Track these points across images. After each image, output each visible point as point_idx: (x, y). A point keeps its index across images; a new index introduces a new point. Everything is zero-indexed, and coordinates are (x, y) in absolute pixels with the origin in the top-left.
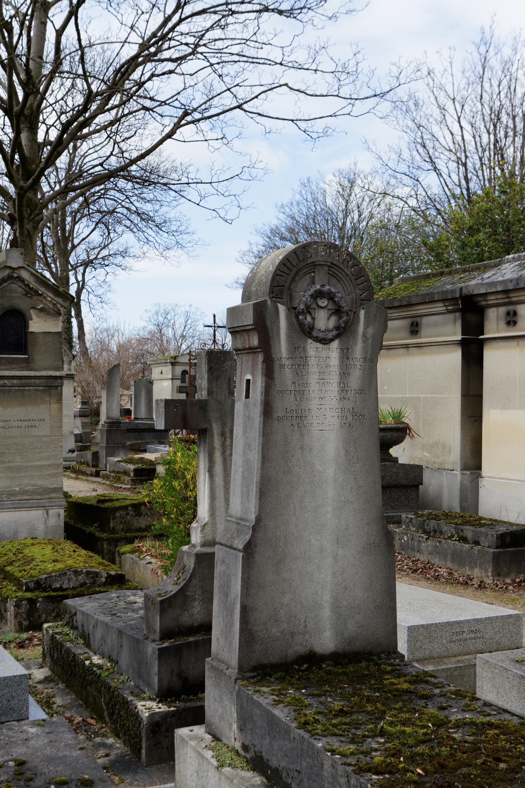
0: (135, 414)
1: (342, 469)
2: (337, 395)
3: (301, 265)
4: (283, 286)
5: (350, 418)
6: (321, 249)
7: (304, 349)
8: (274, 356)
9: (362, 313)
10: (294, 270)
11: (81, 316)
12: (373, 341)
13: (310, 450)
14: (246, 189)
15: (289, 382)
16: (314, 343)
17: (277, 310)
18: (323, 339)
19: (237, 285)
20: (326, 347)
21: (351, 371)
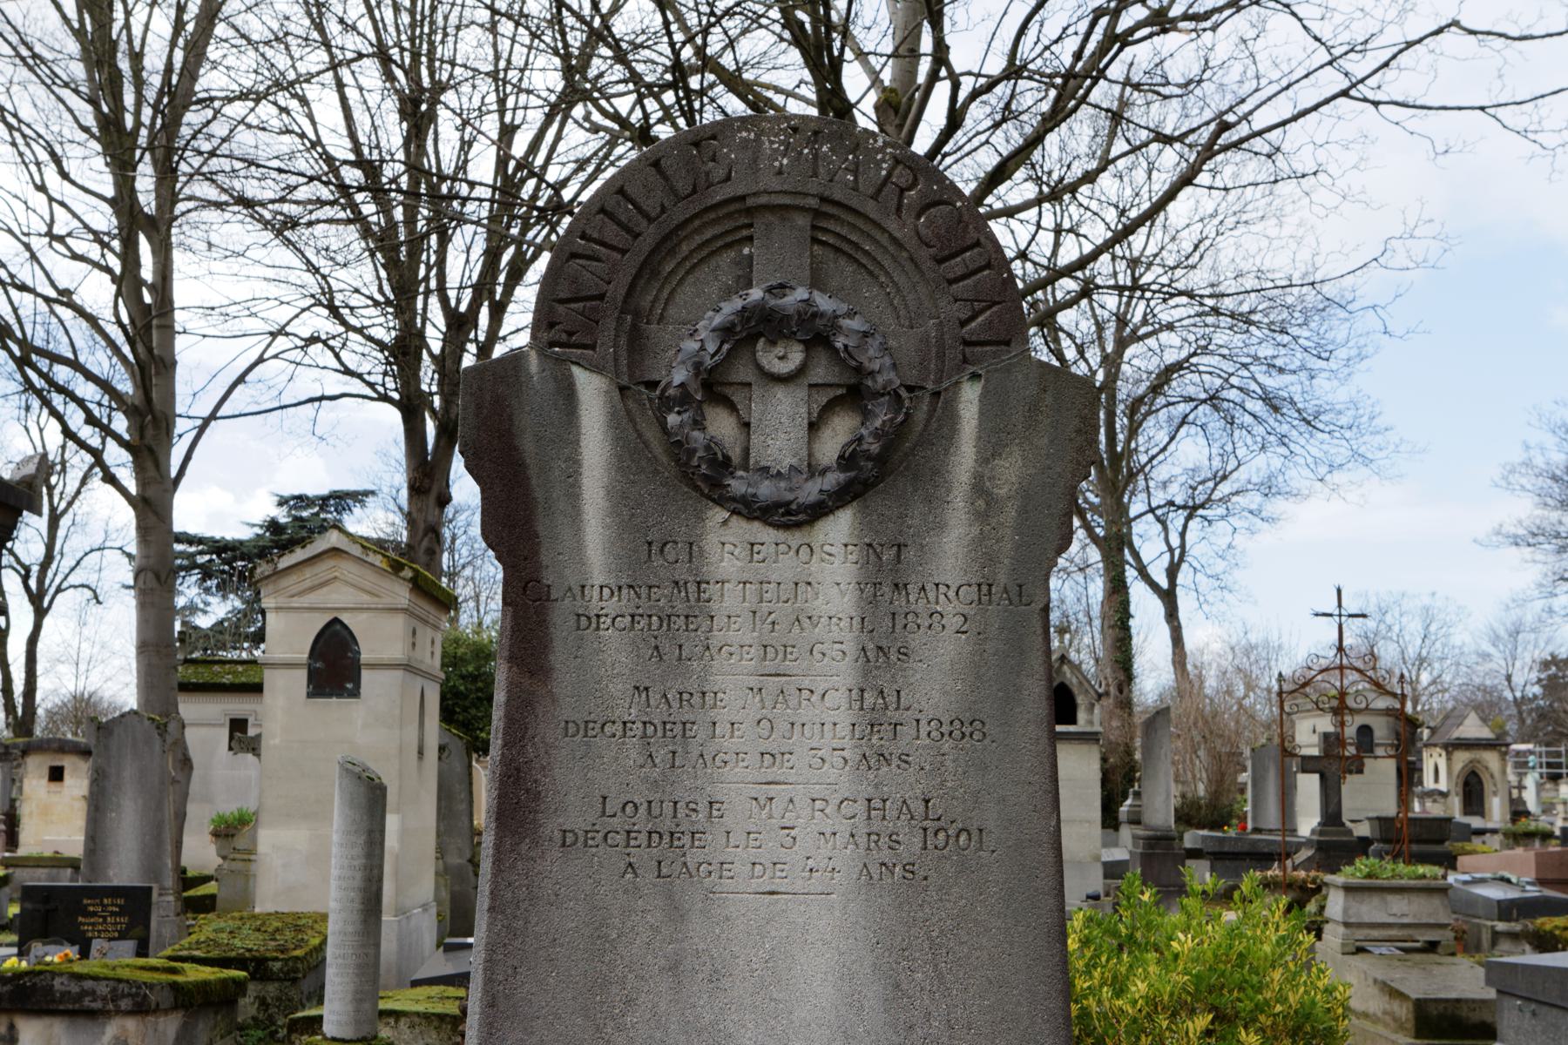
0: (1254, 819)
2: (847, 743)
3: (679, 214)
4: (601, 297)
5: (911, 844)
7: (693, 549)
8: (549, 578)
9: (970, 398)
10: (650, 235)
12: (1023, 511)
13: (715, 977)
14: (1401, 291)
16: (736, 522)
17: (568, 393)
18: (778, 505)
19: (1500, 538)
20: (795, 538)
21: (916, 640)
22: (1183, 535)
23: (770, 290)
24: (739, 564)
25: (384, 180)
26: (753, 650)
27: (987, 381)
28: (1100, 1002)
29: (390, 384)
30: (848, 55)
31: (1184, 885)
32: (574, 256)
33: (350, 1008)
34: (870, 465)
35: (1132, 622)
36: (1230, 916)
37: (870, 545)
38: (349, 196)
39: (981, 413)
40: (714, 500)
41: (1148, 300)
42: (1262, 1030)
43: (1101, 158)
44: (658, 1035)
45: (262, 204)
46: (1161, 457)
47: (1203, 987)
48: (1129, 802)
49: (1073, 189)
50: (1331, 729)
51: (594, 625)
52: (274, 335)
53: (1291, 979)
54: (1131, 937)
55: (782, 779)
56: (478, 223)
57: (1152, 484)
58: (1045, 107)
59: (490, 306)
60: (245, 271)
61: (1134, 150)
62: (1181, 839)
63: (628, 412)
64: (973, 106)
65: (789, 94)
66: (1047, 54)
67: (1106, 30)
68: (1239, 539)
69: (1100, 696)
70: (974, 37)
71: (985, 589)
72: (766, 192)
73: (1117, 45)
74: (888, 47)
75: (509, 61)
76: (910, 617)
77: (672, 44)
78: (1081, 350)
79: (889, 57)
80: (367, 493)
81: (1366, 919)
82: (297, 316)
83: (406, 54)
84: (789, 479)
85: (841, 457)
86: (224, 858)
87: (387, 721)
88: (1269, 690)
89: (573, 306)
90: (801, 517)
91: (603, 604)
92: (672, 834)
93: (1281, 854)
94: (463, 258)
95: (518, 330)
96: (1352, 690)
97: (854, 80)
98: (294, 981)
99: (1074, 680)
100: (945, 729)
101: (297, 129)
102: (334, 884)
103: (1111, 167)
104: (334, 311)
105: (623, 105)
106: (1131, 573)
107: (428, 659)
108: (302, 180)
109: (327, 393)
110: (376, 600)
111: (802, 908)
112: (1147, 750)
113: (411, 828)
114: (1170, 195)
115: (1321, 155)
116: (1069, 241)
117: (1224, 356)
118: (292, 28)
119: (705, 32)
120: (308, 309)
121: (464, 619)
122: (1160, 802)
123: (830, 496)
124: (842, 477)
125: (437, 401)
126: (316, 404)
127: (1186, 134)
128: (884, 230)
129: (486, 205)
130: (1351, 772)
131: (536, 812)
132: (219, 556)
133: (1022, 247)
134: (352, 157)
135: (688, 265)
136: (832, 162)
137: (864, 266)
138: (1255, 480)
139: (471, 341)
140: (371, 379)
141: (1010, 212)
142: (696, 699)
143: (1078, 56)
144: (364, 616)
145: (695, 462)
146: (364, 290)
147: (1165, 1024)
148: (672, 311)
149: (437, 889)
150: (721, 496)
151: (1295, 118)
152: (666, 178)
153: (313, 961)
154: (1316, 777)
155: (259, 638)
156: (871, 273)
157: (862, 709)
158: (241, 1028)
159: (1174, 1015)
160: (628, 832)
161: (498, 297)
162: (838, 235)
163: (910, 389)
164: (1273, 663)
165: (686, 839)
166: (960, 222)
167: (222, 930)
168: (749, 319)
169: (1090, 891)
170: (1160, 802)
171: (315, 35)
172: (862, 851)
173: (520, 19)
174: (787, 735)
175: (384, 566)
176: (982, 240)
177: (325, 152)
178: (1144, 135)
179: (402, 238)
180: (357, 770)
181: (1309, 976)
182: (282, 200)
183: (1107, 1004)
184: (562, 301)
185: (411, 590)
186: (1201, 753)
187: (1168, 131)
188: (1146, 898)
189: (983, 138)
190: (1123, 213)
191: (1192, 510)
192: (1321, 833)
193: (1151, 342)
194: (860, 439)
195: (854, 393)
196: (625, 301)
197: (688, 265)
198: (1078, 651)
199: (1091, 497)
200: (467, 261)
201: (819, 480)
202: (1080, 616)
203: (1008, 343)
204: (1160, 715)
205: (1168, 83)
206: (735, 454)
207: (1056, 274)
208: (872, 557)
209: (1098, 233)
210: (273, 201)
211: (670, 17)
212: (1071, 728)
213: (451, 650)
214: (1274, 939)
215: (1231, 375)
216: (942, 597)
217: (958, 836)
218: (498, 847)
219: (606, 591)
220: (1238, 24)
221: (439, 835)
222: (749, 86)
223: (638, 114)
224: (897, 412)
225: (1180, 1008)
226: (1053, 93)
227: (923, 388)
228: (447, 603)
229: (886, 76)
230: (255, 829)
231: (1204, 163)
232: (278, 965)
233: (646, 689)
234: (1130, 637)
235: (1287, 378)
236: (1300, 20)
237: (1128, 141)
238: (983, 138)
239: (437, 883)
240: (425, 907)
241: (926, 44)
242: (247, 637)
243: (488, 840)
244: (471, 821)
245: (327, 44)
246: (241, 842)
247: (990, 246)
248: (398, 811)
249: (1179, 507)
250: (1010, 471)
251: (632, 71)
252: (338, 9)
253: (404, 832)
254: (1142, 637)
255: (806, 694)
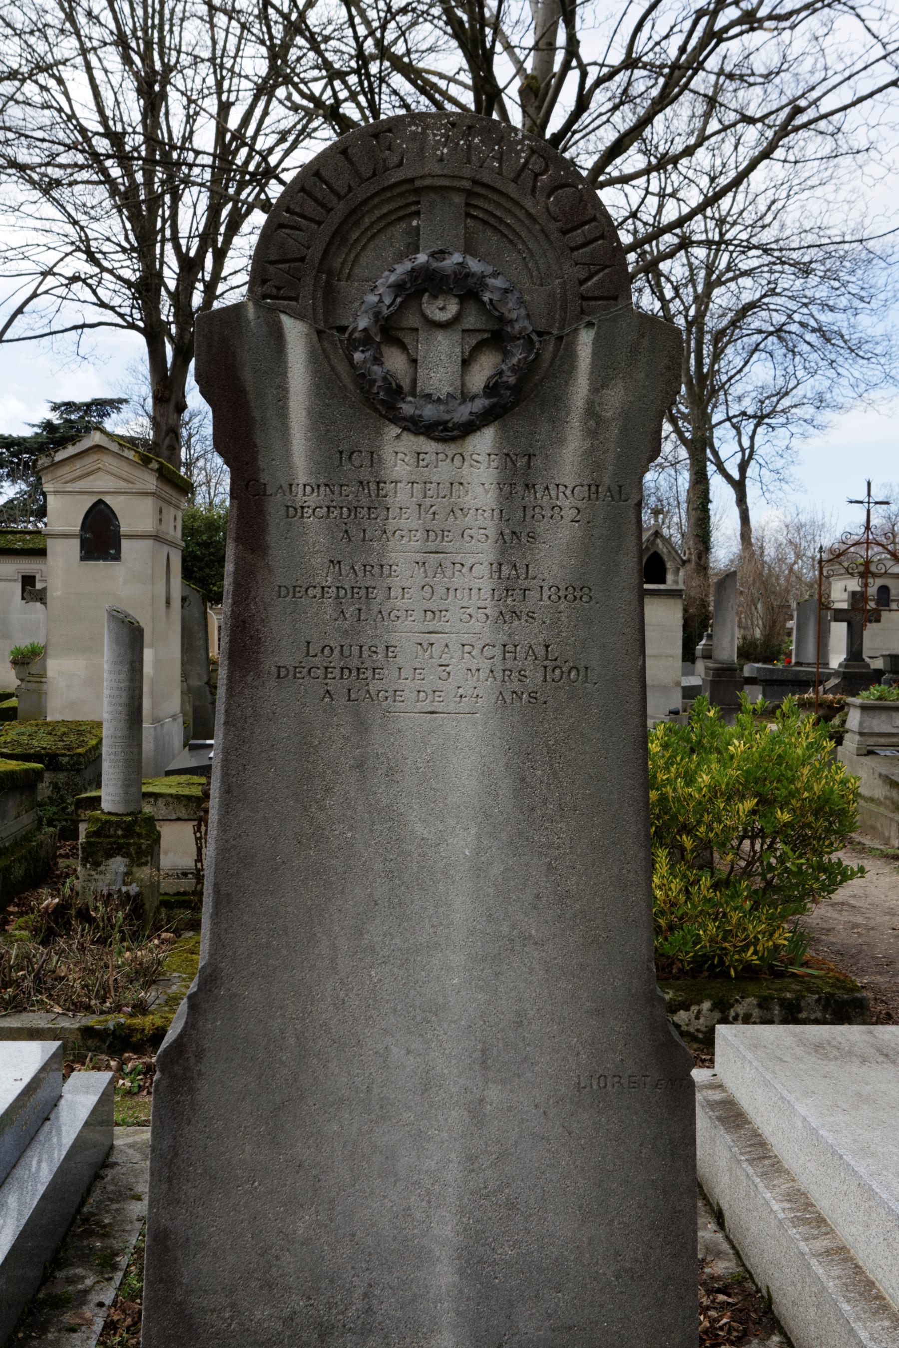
0: (797, 655)
1: (504, 836)
2: (489, 603)
3: (362, 193)
4: (302, 259)
5: (535, 677)
6: (435, 136)
7: (374, 458)
8: (265, 478)
9: (585, 341)
10: (340, 209)
11: (745, 503)
12: (624, 430)
13: (390, 772)
15: (318, 561)
16: (406, 436)
17: (278, 336)
20: (451, 449)
21: (541, 527)
22: (752, 438)
23: (432, 255)
24: (408, 468)
25: (128, 148)
26: (419, 534)
27: (599, 328)
28: (675, 790)
29: (137, 316)
30: (499, 47)
31: (741, 705)
32: (281, 226)
33: (121, 791)
34: (508, 393)
35: (710, 506)
36: (773, 727)
37: (507, 455)
38: (100, 163)
39: (594, 353)
40: (389, 420)
41: (731, 252)
42: (794, 810)
43: (698, 136)
44: (349, 813)
45: (32, 169)
46: (738, 377)
47: (751, 779)
48: (703, 642)
49: (675, 160)
50: (858, 589)
51: (299, 514)
52: (44, 274)
53: (816, 773)
54: (699, 742)
55: (440, 629)
56: (202, 185)
57: (730, 398)
58: (655, 92)
59: (213, 252)
60: (20, 223)
61: (725, 128)
62: (742, 670)
63: (324, 350)
64: (598, 91)
65: (451, 80)
66: (657, 49)
67: (705, 29)
68: (795, 442)
69: (684, 563)
70: (599, 36)
71: (593, 488)
72: (430, 175)
73: (714, 41)
74: (529, 40)
75: (224, 49)
76: (537, 510)
77: (356, 37)
78: (676, 289)
79: (531, 50)
80: (122, 401)
81: (876, 730)
82: (62, 260)
83: (141, 41)
84: (447, 403)
85: (486, 387)
86: (22, 680)
87: (142, 580)
88: (813, 558)
89: (281, 266)
90: (455, 433)
91: (306, 498)
92: (358, 669)
93: (817, 681)
94: (191, 211)
95: (235, 272)
96: (875, 559)
97: (503, 69)
98: (78, 771)
99: (665, 550)
100: (561, 593)
101: (55, 104)
102: (106, 701)
103: (706, 143)
104: (92, 258)
105: (317, 88)
106: (711, 468)
107: (172, 532)
108: (62, 148)
109: (88, 322)
110: (130, 485)
111: (454, 724)
112: (718, 603)
113: (162, 658)
114: (753, 165)
115: (873, 135)
116: (671, 204)
117: (789, 297)
118: (49, 19)
119: (383, 27)
120: (71, 253)
121: (199, 500)
122: (727, 642)
123: (477, 417)
124: (487, 402)
125: (173, 329)
126: (79, 331)
127: (767, 116)
128: (522, 207)
129: (209, 170)
130: (870, 622)
131: (258, 653)
132: (8, 450)
133: (634, 208)
134: (101, 130)
135: (369, 234)
136: (482, 151)
137: (506, 236)
138: (809, 395)
139: (199, 281)
140: (122, 311)
141: (625, 179)
142: (376, 570)
143: (682, 49)
144: (122, 498)
145: (375, 390)
146: (113, 239)
147: (722, 806)
148: (357, 271)
149: (183, 704)
150: (395, 416)
151: (854, 104)
152: (352, 164)
153: (91, 756)
154: (845, 624)
155: (42, 513)
156: (511, 241)
157: (500, 578)
158: (40, 805)
159: (729, 800)
160: (326, 668)
161: (219, 245)
162: (486, 211)
163: (540, 334)
164: (817, 538)
165: (369, 673)
166: (581, 201)
167: (23, 734)
168: (416, 278)
169: (672, 708)
170: (727, 642)
171: (68, 25)
172: (498, 682)
173: (232, 13)
174: (444, 597)
175: (136, 459)
176: (598, 215)
177: (79, 124)
178: (732, 117)
179: (142, 197)
180: (121, 616)
181: (830, 771)
182: (48, 164)
183: (680, 791)
184: (272, 263)
185: (158, 478)
186: (759, 606)
187: (749, 113)
188: (711, 714)
189: (604, 118)
190: (713, 180)
191: (760, 419)
192: (846, 666)
193: (732, 285)
194: (501, 373)
195: (497, 338)
196: (321, 263)
197: (369, 234)
198: (669, 528)
199: (682, 408)
200: (195, 214)
201: (470, 404)
202: (671, 500)
203: (615, 298)
204: (729, 577)
205: (753, 74)
206: (406, 384)
207: (659, 231)
208: (509, 464)
209: (694, 198)
210: (40, 165)
211: (354, 11)
212: (662, 587)
213: (189, 523)
214: (805, 744)
215: (795, 312)
216: (561, 495)
217: (569, 672)
218: (230, 678)
219: (308, 488)
220: (812, 23)
221: (183, 664)
222: (419, 72)
223: (329, 92)
224: (530, 352)
225: (733, 794)
226: (661, 81)
227: (549, 333)
228: (186, 488)
229: (529, 65)
230: (44, 659)
231: (780, 139)
232: (66, 759)
233: (339, 562)
234: (709, 518)
235: (839, 316)
236: (863, 20)
237: (720, 121)
238: (604, 118)
239: (182, 699)
240: (174, 717)
241: (561, 38)
242: (32, 513)
243: (222, 674)
244: (207, 654)
245: (78, 34)
246: (34, 669)
247: (603, 221)
248: (152, 646)
249: (750, 417)
250: (615, 398)
251: (325, 60)
252: (84, 4)
253: (157, 662)
254: (718, 517)
255: (458, 566)
